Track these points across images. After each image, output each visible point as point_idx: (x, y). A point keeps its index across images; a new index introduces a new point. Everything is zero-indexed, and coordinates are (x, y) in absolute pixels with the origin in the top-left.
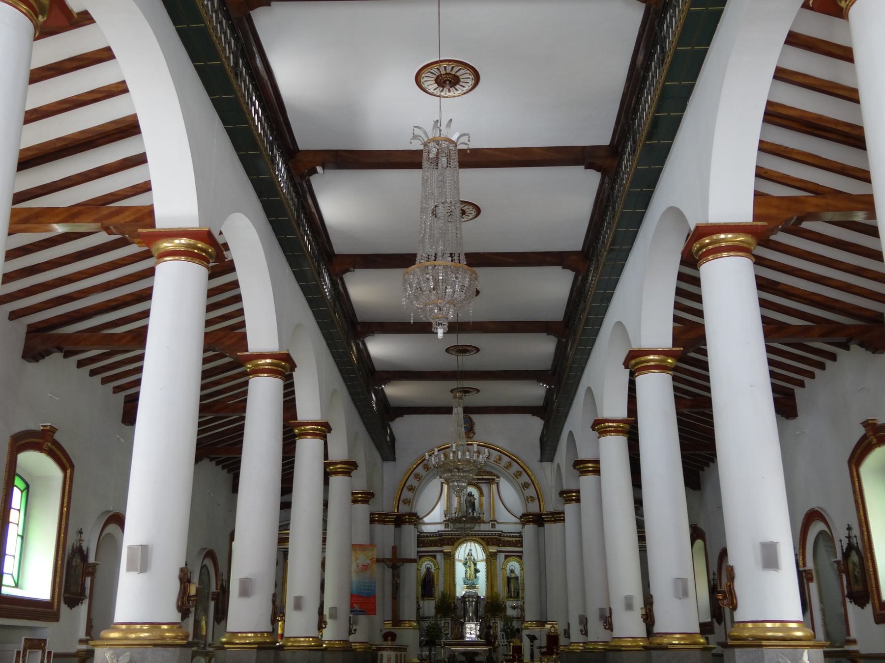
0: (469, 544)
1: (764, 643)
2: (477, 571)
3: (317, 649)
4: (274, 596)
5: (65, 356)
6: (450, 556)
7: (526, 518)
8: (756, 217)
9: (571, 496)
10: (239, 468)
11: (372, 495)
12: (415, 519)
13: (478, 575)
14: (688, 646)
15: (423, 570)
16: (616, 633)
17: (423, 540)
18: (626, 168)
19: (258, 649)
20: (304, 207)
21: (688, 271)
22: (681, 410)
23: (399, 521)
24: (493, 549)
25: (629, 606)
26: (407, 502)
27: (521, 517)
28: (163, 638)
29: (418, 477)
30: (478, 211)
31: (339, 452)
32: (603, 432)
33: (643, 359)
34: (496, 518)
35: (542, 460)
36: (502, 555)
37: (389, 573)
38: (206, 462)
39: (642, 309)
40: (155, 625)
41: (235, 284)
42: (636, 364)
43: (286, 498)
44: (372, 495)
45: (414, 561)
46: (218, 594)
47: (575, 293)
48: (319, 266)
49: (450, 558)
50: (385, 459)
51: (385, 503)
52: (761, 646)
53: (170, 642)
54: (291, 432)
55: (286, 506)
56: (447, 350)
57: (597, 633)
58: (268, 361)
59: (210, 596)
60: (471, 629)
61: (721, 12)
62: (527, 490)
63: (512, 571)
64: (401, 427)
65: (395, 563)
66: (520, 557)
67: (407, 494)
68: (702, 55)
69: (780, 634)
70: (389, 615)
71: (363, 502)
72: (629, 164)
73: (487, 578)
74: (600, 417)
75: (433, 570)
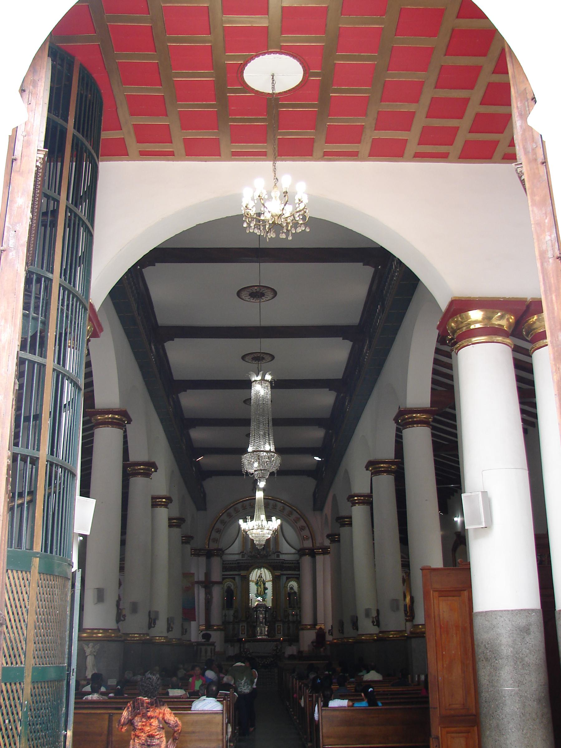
2: (265, 589)
7: (302, 552)
9: (334, 538)
11: (192, 537)
12: (220, 552)
13: (266, 591)
15: (225, 588)
16: (360, 632)
17: (227, 567)
24: (278, 573)
26: (216, 540)
28: (111, 637)
30: (275, 293)
32: (354, 504)
33: (377, 466)
34: (280, 550)
36: (284, 578)
44: (192, 537)
49: (246, 580)
50: (198, 509)
53: (114, 638)
56: (243, 358)
60: (260, 582)
63: (292, 588)
64: (210, 484)
66: (298, 579)
67: (214, 535)
70: (202, 621)
73: (273, 593)
74: (353, 493)
75: (232, 588)
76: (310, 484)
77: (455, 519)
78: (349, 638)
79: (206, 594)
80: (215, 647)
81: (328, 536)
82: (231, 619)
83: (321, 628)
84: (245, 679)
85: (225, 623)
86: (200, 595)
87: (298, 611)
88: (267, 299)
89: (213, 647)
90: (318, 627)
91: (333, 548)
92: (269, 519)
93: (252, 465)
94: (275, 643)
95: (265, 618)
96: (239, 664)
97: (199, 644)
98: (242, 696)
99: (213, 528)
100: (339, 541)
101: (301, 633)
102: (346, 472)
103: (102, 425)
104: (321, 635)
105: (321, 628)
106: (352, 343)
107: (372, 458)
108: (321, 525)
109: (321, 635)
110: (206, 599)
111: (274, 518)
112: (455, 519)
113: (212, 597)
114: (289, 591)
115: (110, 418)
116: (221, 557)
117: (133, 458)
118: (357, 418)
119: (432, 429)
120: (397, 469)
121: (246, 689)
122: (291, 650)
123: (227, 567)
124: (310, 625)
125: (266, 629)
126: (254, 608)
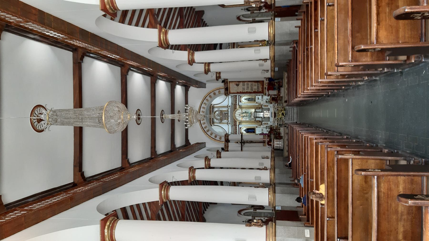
2: (246, 112)
4: (255, 187)
10: (208, 203)
16: (268, 58)
20: (99, 180)
23: (227, 141)
24: (238, 106)
29: (211, 134)
30: (138, 110)
31: (201, 163)
33: (162, 41)
36: (240, 103)
37: (246, 145)
38: (206, 215)
39: (176, 59)
41: (132, 207)
42: (164, 44)
43: (219, 183)
45: (242, 135)
46: (254, 209)
54: (193, 182)
55: (222, 183)
58: (163, 192)
59: (254, 18)
64: (192, 141)
65: (243, 142)
67: (218, 138)
71: (220, 154)
75: (245, 129)
106: (85, 57)
117: (204, 167)
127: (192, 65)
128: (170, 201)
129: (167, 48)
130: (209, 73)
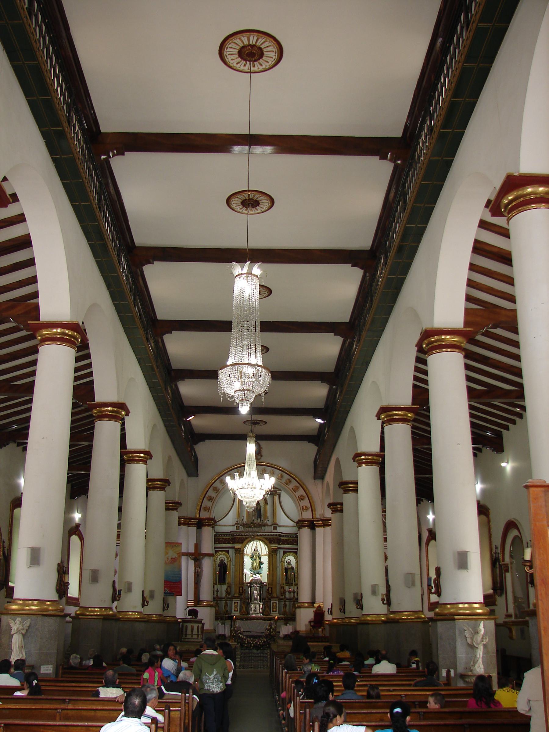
0: (255, 542)
1: (456, 617)
2: (261, 563)
3: (145, 620)
5: (18, 446)
6: (240, 551)
8: (466, 323)
9: (336, 507)
13: (262, 566)
14: (413, 620)
15: (218, 562)
16: (365, 612)
18: (381, 274)
19: (103, 619)
21: (422, 356)
22: (418, 447)
24: (274, 546)
25: (374, 592)
26: (207, 509)
27: (297, 523)
28: (48, 610)
31: (158, 473)
32: (360, 464)
34: (277, 522)
35: (315, 478)
39: (387, 379)
40: (42, 602)
47: (343, 353)
48: (147, 333)
49: (240, 553)
50: (189, 475)
51: (189, 509)
52: (455, 620)
53: (52, 613)
57: (352, 610)
58: (158, 483)
61: (442, 185)
62: (302, 502)
63: (289, 563)
64: (203, 449)
66: (295, 553)
67: (206, 503)
68: (432, 209)
69: (467, 611)
70: (191, 596)
72: (424, 144)
73: (269, 569)
74: (359, 451)
75: (226, 562)
76: (311, 450)
77: (503, 464)
78: (351, 618)
79: (195, 567)
80: (203, 624)
81: (330, 505)
82: (224, 595)
83: (319, 607)
84: (215, 673)
85: (216, 599)
86: (187, 568)
87: (296, 587)
88: (263, 210)
89: (200, 625)
90: (316, 605)
91: (334, 518)
92: (261, 475)
93: (231, 384)
94: (269, 622)
95: (260, 594)
96: (210, 651)
97: (184, 621)
98: (207, 698)
99: (205, 496)
100: (342, 511)
101: (298, 610)
102: (352, 428)
103: (46, 341)
104: (319, 614)
105: (319, 607)
107: (385, 404)
108: (321, 494)
109: (319, 614)
110: (195, 573)
111: (267, 476)
112: (503, 464)
113: (202, 570)
114: (286, 566)
115: (59, 333)
116: (213, 527)
118: (366, 363)
119: (466, 357)
120: (419, 414)
121: (214, 686)
122: (285, 630)
123: (218, 539)
124: (307, 603)
125: (261, 606)
126: (248, 583)
127: (354, 459)
128: (35, 350)
129: (420, 350)
130: (342, 491)
